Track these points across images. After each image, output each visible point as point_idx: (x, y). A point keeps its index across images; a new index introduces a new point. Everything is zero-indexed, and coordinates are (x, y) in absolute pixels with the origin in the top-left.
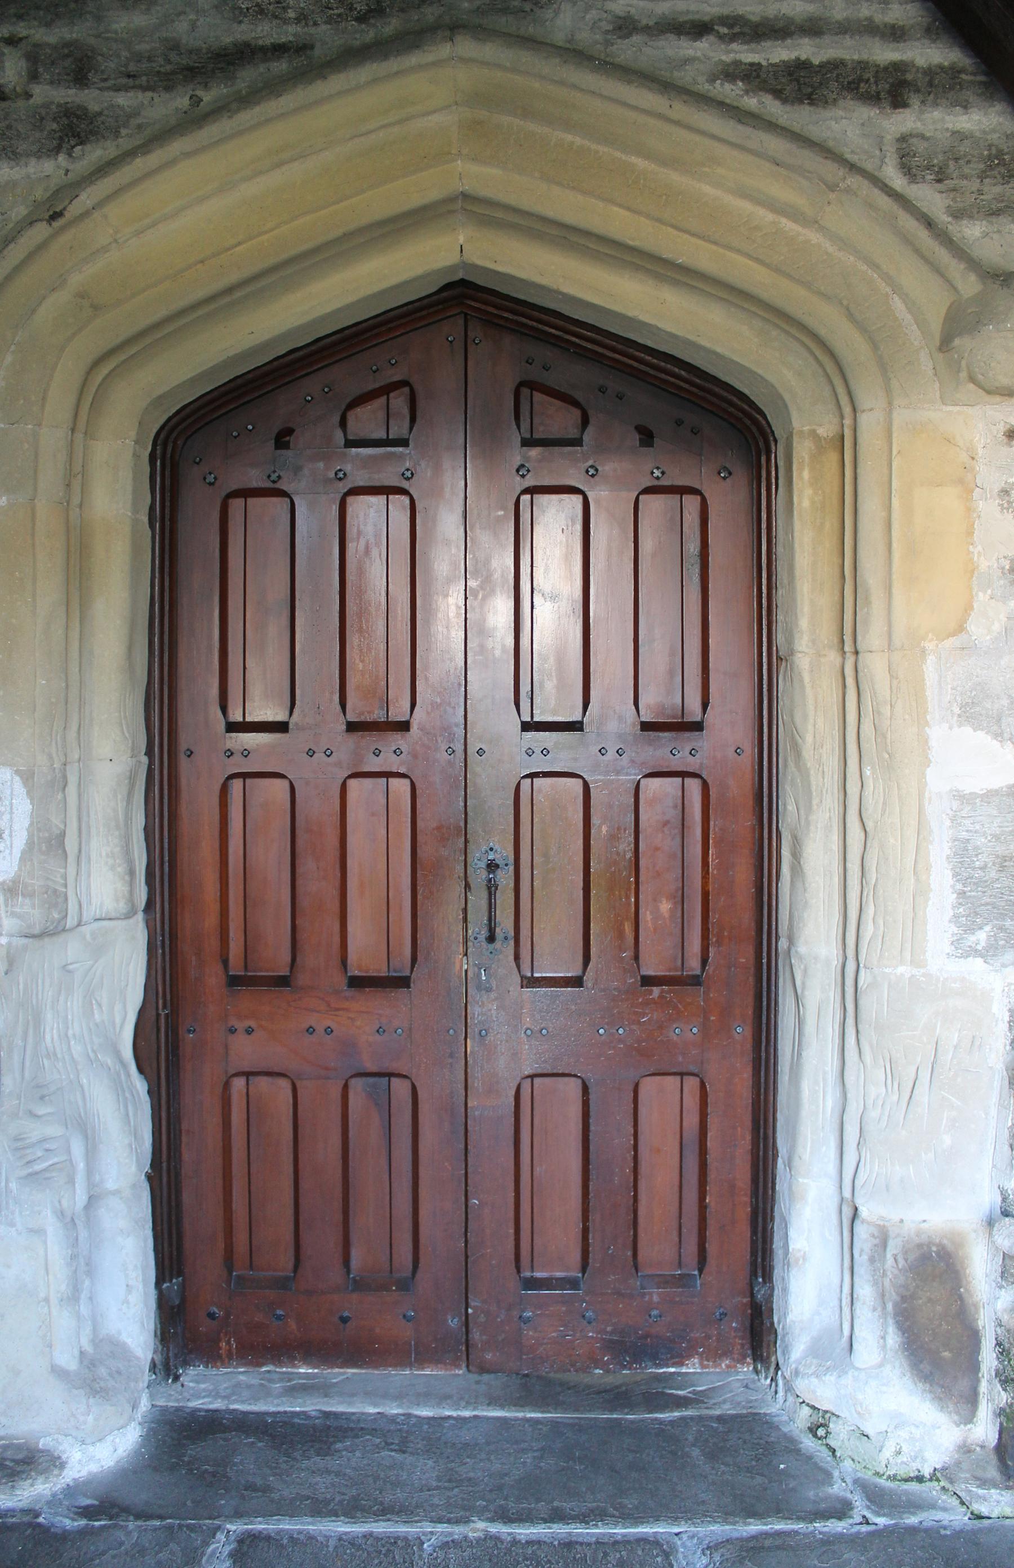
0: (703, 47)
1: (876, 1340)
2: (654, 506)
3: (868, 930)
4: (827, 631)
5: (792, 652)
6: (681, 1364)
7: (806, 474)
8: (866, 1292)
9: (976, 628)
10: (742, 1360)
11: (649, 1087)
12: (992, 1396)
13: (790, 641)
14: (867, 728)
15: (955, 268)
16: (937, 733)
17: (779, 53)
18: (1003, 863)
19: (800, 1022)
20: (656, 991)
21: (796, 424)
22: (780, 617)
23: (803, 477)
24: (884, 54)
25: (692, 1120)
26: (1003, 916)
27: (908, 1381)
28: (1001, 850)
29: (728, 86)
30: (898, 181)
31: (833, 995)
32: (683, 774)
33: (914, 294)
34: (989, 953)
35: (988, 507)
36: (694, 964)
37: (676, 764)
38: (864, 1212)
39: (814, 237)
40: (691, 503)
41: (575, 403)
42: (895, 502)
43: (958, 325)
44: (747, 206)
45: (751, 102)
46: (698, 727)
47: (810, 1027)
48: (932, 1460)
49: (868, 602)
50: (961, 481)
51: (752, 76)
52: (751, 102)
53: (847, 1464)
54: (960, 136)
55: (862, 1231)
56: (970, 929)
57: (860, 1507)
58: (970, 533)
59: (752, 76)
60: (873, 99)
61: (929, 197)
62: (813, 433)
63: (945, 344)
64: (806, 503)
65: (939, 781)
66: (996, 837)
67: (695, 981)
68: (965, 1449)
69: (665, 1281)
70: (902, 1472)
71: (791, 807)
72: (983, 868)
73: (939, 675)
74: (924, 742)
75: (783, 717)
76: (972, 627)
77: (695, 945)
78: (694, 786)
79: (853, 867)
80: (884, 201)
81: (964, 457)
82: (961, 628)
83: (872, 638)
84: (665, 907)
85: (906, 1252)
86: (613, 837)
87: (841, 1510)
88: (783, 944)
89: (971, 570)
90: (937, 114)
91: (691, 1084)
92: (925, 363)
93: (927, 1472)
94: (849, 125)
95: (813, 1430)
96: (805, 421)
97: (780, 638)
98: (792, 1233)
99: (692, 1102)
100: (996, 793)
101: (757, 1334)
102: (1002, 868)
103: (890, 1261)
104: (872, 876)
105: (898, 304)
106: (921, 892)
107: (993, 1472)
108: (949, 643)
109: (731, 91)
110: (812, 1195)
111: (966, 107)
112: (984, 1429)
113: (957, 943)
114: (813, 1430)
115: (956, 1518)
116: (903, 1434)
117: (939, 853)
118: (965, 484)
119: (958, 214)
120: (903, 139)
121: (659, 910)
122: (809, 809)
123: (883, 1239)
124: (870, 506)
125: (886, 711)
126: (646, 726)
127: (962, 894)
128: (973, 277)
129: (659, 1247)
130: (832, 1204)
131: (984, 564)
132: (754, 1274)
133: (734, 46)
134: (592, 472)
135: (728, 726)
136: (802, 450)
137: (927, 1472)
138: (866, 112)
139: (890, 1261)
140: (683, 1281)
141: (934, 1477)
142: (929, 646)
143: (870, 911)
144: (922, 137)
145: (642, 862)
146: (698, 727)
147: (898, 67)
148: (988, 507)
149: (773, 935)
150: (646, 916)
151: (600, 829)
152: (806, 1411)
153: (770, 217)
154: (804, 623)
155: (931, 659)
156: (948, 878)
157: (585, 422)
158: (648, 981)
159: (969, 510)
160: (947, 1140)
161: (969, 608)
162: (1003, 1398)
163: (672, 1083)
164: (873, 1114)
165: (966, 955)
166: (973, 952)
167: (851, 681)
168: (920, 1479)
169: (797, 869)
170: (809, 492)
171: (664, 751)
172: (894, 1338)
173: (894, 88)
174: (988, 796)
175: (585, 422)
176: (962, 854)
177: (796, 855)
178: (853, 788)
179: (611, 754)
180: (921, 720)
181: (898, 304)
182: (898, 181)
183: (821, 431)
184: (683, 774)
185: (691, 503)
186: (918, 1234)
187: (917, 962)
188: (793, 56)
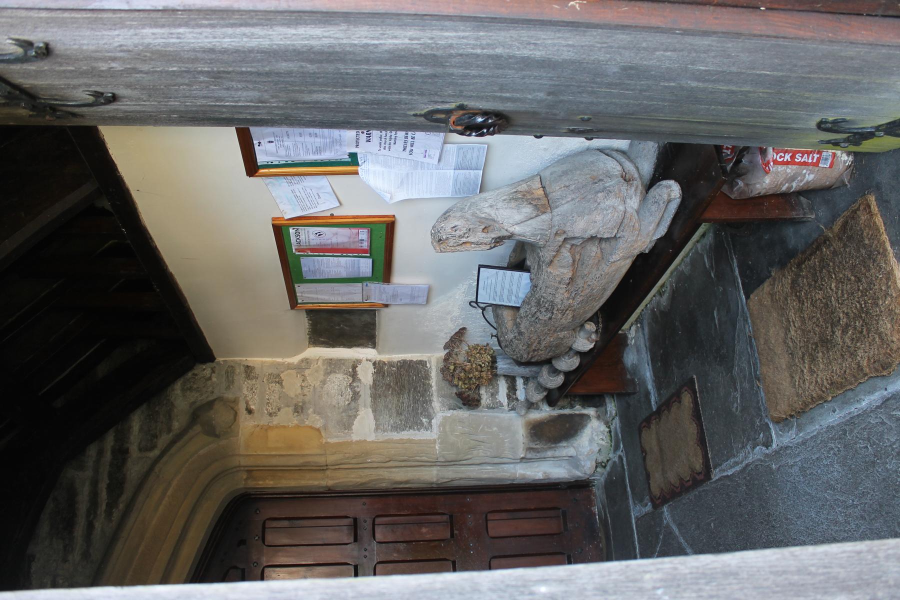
0: (98, 525)
1: (567, 450)
2: (270, 538)
3: (424, 458)
4: (320, 475)
5: (327, 487)
6: (595, 514)
7: (261, 482)
8: (550, 453)
9: (318, 425)
10: (591, 491)
11: (492, 533)
12: (578, 410)
13: (322, 487)
14: (353, 461)
15: (191, 433)
16: (355, 438)
17: (104, 495)
18: (399, 414)
19: (461, 479)
20: (456, 532)
21: (242, 486)
22: (313, 490)
23: (261, 484)
24: (108, 456)
25: (504, 516)
26: (417, 413)
27: (577, 438)
28: (395, 415)
29: (114, 515)
30: (156, 452)
31: (450, 468)
32: (374, 525)
33: (198, 446)
34: (430, 418)
35: (276, 421)
36: (445, 518)
37: (369, 528)
38: (522, 456)
39: (175, 483)
40: (270, 524)
41: (228, 571)
42: (274, 453)
43: (212, 432)
44: (161, 508)
45: (121, 506)
46: (355, 520)
47: (463, 476)
48: (603, 428)
49: (309, 462)
50: (266, 430)
51: (111, 506)
52: (121, 506)
53: (611, 456)
54: (141, 429)
55: (529, 456)
56: (422, 424)
57: (619, 453)
58: (284, 427)
59: (111, 506)
60: (124, 461)
61: (163, 440)
62: (246, 480)
63: (217, 436)
64: (272, 482)
65: (372, 437)
66: (390, 416)
67: (451, 517)
68: (598, 417)
69: (565, 523)
70: (609, 438)
71: (384, 485)
72: (401, 420)
73: (334, 438)
74: (358, 442)
75: (351, 488)
76: (318, 426)
77: (438, 518)
78: (378, 520)
79: (403, 464)
80: (165, 459)
81: (258, 429)
82: (318, 430)
83: (321, 460)
84: (424, 530)
85: (534, 441)
86: (398, 551)
87: (620, 458)
88: (434, 486)
89: (297, 426)
90: (132, 438)
91: (490, 516)
92: (223, 442)
93: (607, 430)
94: (134, 470)
95: (605, 467)
96: (241, 483)
97: (321, 490)
98: (537, 478)
99: (497, 516)
100: (375, 416)
101: (580, 486)
102: (401, 414)
103: (538, 446)
104: (405, 458)
105: (202, 452)
106: (410, 441)
107: (603, 409)
108: (323, 434)
109: (116, 515)
110: (522, 472)
111: (130, 427)
112: (591, 411)
113: (427, 429)
114: (605, 467)
115: (617, 420)
116: (596, 438)
117: (396, 436)
118: (267, 428)
119: (169, 430)
120: (140, 450)
121: (426, 532)
122: (383, 479)
123: (530, 449)
124: (274, 462)
125: (347, 455)
126: (356, 540)
127: (410, 428)
128: (195, 428)
129: (552, 526)
130: (524, 465)
131: (296, 422)
132: (558, 489)
133: (99, 513)
134: (257, 563)
135: (357, 508)
136: (251, 484)
137: (607, 430)
138: (129, 463)
139: (538, 446)
140: (564, 514)
141: (609, 427)
142: (324, 441)
143: (418, 458)
144: (140, 443)
145: (408, 539)
146: (355, 520)
147: (113, 452)
148: (276, 421)
149: (432, 489)
150: (428, 537)
151: (395, 556)
152: (598, 469)
153: (166, 499)
154: (316, 483)
155: (329, 440)
156: (405, 433)
157: (236, 568)
158: (452, 535)
159: (276, 427)
160: (495, 429)
161: (311, 427)
162: (578, 407)
163: (490, 524)
164: (489, 454)
165: (431, 426)
166: (430, 423)
167: (337, 466)
168: (610, 432)
169: (407, 482)
170: (267, 481)
171: (365, 534)
172: (564, 444)
173: (121, 453)
174: (376, 419)
175: (236, 568)
176: (396, 428)
177: (401, 483)
178: (375, 465)
179: (366, 553)
180: (351, 443)
181: (202, 452)
182: (156, 452)
183: (245, 477)
184: (374, 525)
185: (270, 524)
186: (527, 437)
187: (434, 441)
188: (105, 490)
